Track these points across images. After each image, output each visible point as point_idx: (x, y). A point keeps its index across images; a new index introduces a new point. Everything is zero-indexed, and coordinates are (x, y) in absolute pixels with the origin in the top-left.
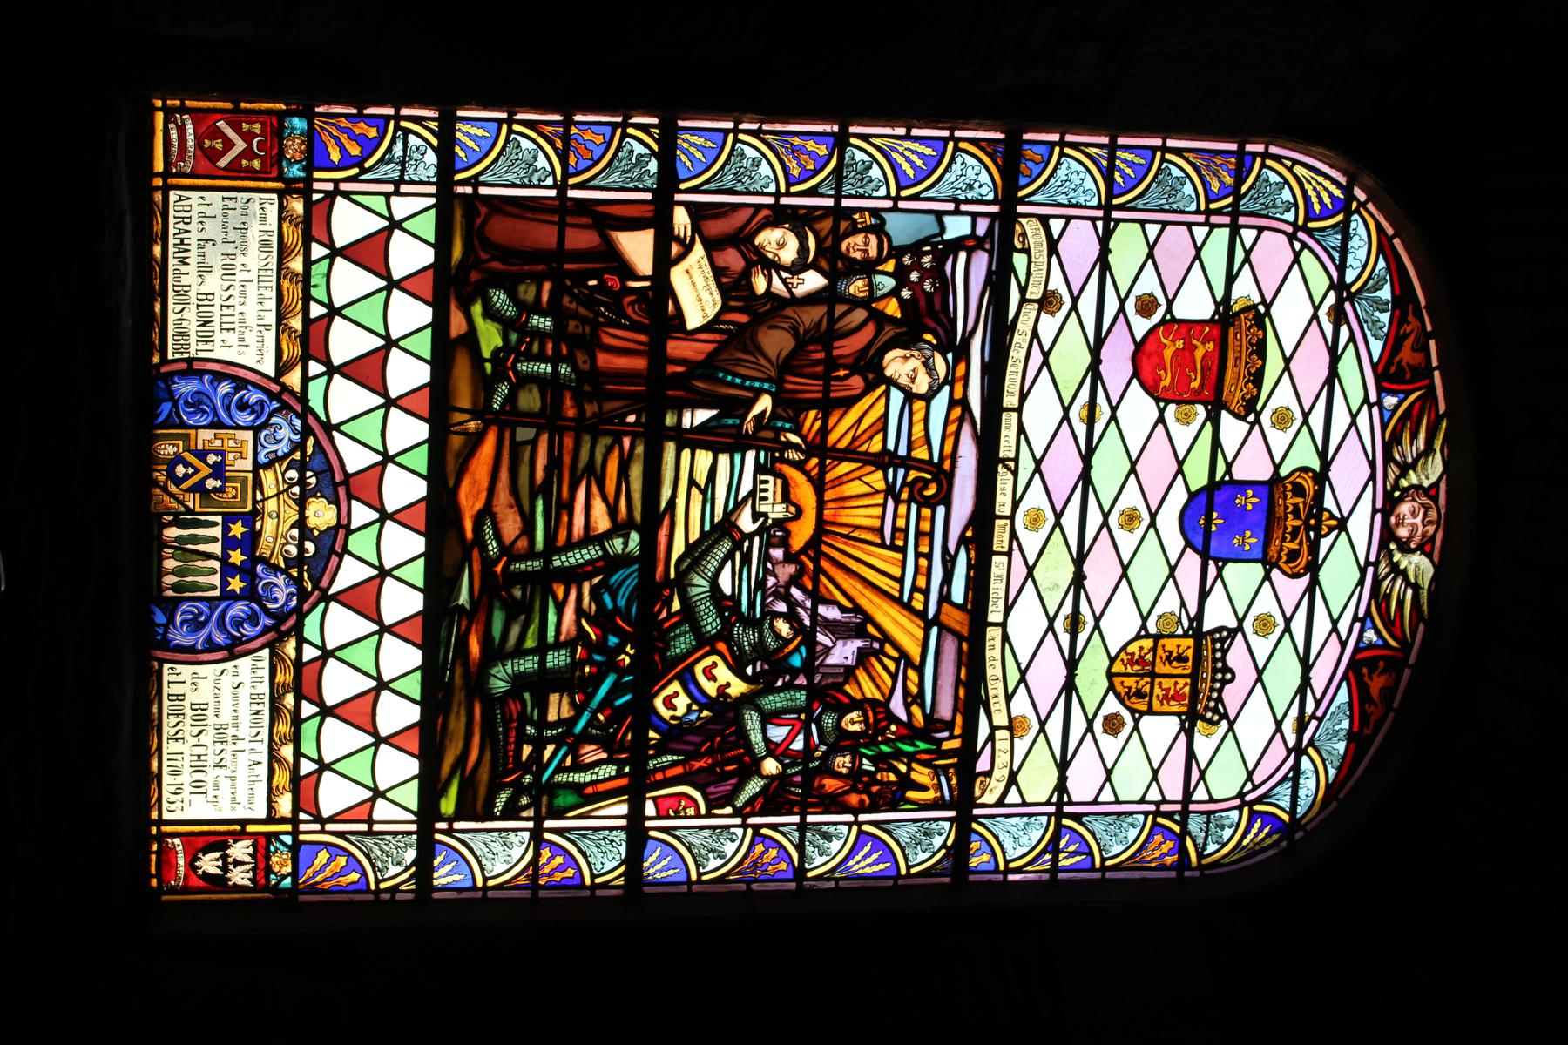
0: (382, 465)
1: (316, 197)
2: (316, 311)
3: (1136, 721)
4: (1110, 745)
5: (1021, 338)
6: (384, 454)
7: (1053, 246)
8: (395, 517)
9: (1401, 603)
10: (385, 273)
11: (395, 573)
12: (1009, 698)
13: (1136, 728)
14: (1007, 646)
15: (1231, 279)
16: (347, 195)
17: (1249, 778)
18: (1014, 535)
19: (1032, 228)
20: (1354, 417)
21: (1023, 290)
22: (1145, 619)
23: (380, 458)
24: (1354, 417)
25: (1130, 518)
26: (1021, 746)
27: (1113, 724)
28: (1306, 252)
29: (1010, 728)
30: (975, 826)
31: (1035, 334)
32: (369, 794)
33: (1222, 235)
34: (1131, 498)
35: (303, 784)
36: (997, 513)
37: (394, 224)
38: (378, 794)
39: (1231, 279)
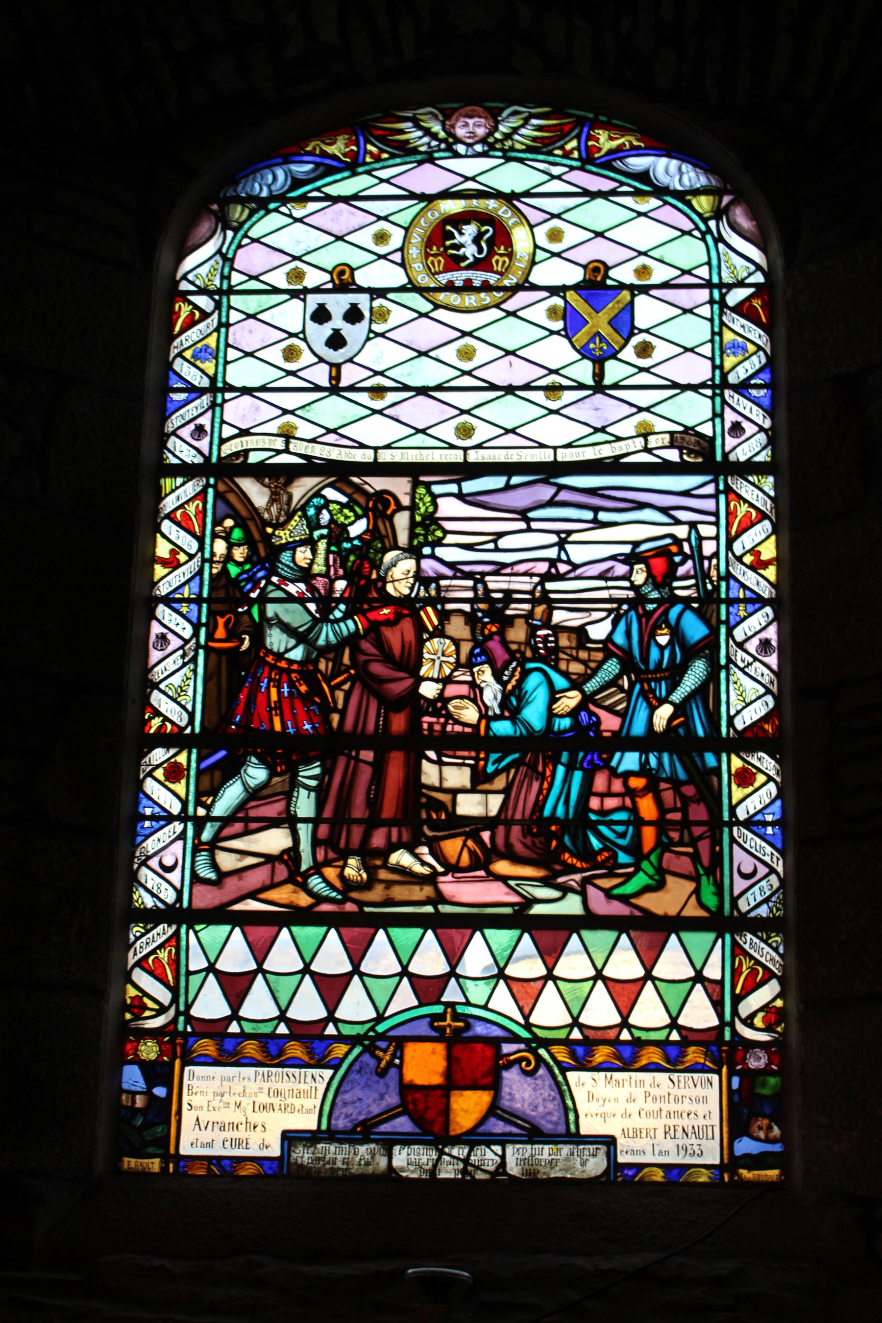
0: (606, 980)
1: (189, 1029)
2: (283, 1029)
3: (641, 331)
4: (662, 350)
5: (317, 451)
6: (595, 979)
7: (244, 433)
8: (550, 967)
9: (540, 128)
10: (348, 976)
11: (405, 963)
12: (619, 439)
13: (647, 331)
14: (447, 446)
15: (275, 291)
16: (189, 1006)
17: (689, 233)
18: (479, 446)
19: (228, 449)
20: (382, 181)
21: (278, 452)
22: (552, 333)
23: (502, 982)
24: (382, 181)
25: (466, 354)
26: (660, 425)
27: (644, 350)
28: (250, 234)
29: (645, 436)
30: (214, 460)
31: (313, 441)
32: (600, 983)
33: (235, 300)
34: (449, 354)
35: (198, 1030)
36: (372, 460)
37: (211, 968)
38: (699, 978)
39: (275, 291)
